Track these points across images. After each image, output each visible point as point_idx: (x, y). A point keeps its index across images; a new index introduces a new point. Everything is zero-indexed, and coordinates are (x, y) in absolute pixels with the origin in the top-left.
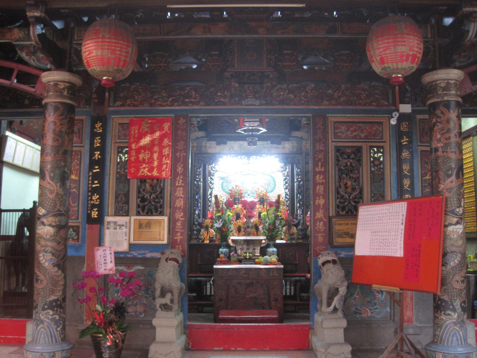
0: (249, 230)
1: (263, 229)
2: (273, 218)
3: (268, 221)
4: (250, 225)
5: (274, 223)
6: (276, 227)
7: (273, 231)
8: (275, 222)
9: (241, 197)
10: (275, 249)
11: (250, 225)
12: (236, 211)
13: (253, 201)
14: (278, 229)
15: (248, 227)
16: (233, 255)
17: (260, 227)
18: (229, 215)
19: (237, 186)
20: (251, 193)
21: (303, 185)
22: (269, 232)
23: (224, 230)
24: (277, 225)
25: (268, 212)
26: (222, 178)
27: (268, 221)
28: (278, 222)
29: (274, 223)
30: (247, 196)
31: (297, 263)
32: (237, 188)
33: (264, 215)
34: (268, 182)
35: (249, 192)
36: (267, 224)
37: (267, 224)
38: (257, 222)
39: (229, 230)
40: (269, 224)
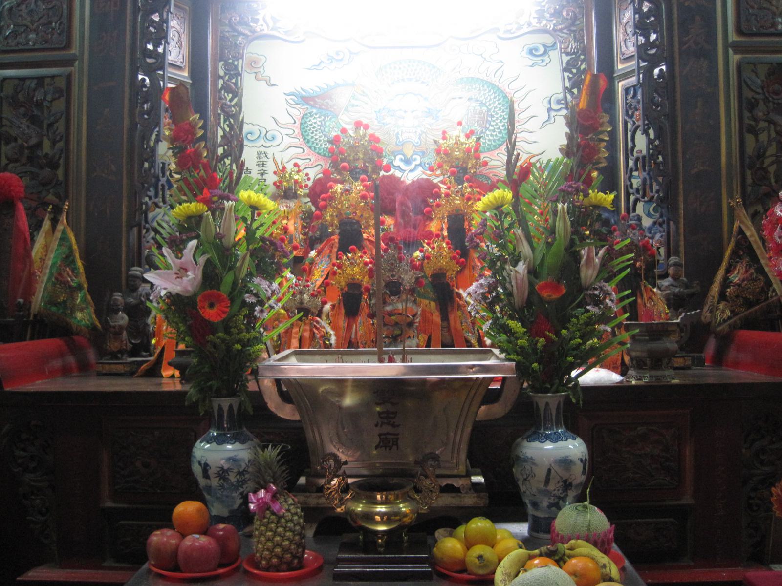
0: (400, 306)
1: (490, 307)
2: (563, 226)
3: (525, 249)
4: (408, 278)
5: (571, 261)
6: (581, 289)
7: (564, 321)
8: (576, 257)
9: (378, 167)
10: (574, 447)
11: (408, 278)
12: (340, 214)
13: (428, 181)
14: (597, 302)
15: (394, 288)
16: (264, 507)
17: (470, 293)
18: (255, 208)
19: (358, 124)
20: (415, 153)
21: (669, 77)
22: (533, 331)
23: (211, 314)
24: (588, 274)
25: (521, 191)
26: (306, 99)
27: (525, 249)
28: (592, 257)
29: (571, 261)
30: (403, 166)
31: (687, 500)
32: (362, 131)
33: (498, 207)
34: (484, 109)
35: (409, 152)
36: (521, 267)
37: (521, 267)
38: (443, 262)
39: (251, 319)
40: (533, 272)
